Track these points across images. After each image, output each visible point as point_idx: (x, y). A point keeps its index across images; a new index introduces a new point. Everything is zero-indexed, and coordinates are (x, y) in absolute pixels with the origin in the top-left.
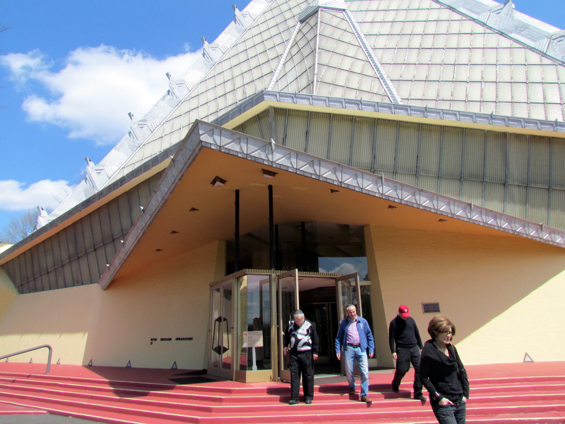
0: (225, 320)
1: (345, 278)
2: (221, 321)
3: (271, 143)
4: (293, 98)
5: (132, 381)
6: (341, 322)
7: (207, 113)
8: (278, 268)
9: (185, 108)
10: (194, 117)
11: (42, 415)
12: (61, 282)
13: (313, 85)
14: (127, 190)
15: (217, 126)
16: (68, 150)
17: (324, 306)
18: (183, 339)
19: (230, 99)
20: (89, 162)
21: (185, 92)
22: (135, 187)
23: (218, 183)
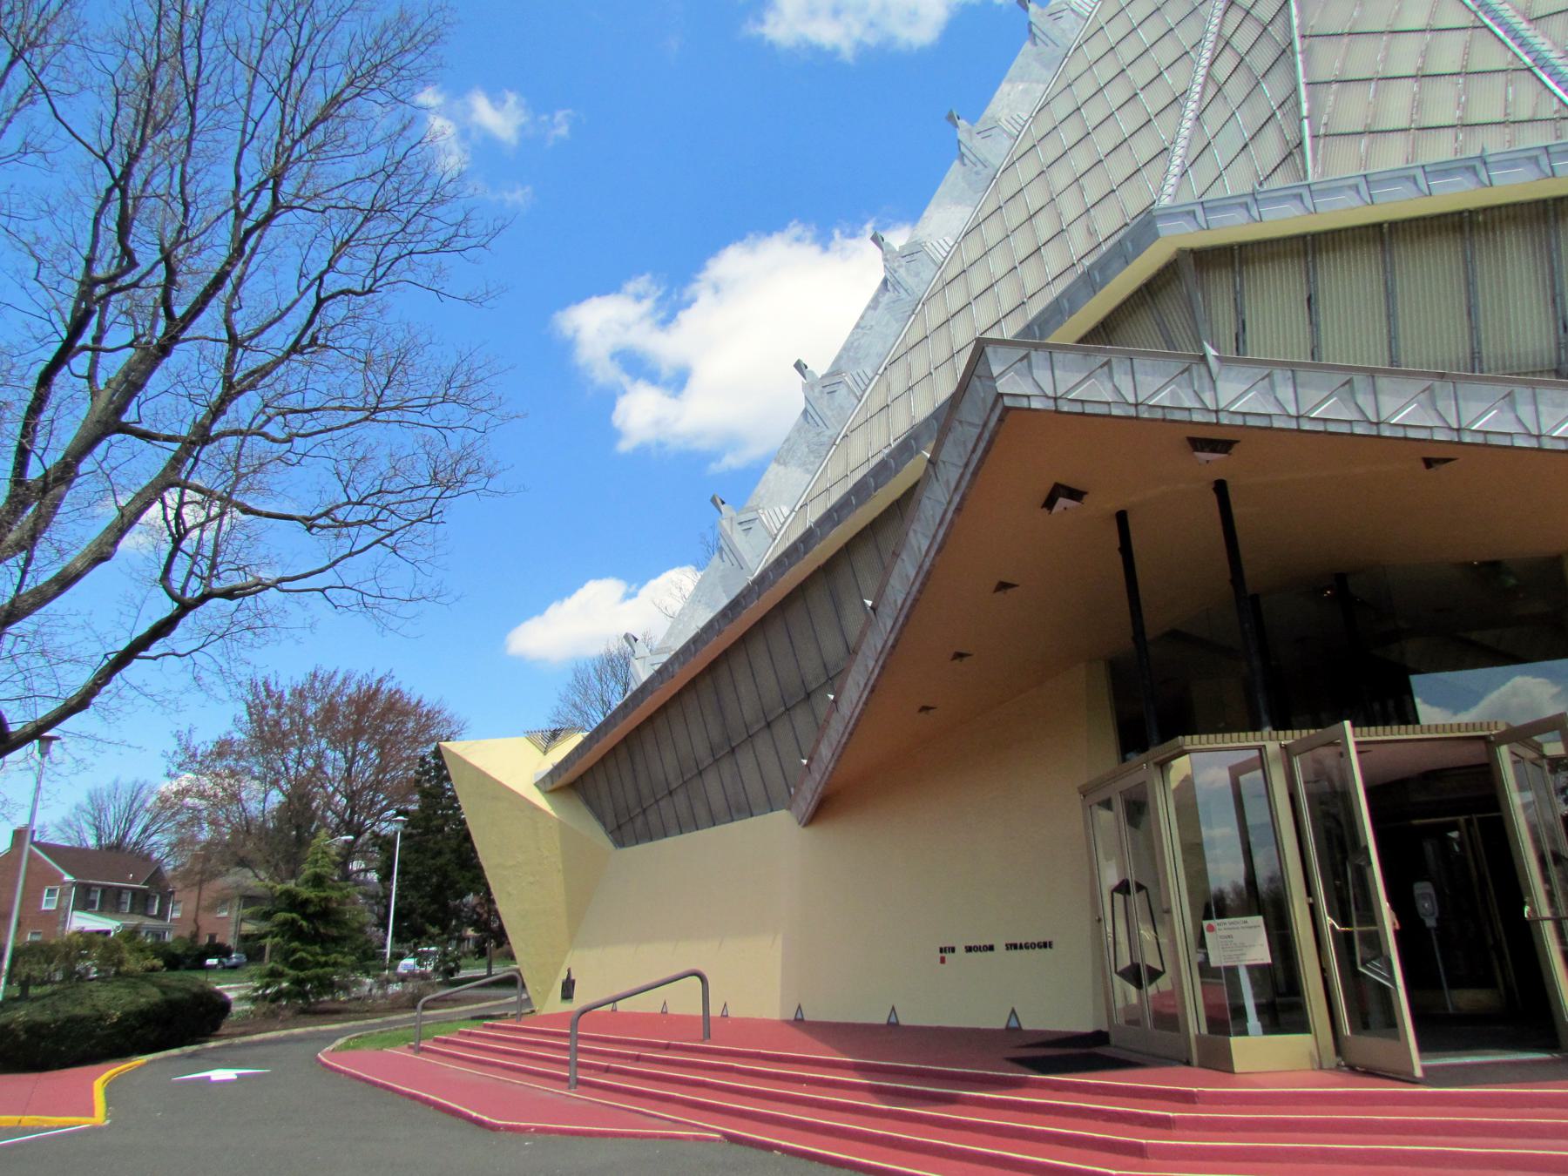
0: (1140, 887)
1: (1522, 735)
2: (1128, 892)
3: (1203, 358)
4: (1246, 206)
5: (915, 1063)
6: (1431, 922)
7: (999, 313)
8: (1282, 724)
9: (935, 315)
10: (963, 335)
11: (712, 1144)
12: (701, 812)
13: (1303, 154)
14: (822, 561)
15: (1034, 340)
16: (693, 489)
17: (1454, 826)
18: (1027, 946)
19: (1054, 260)
20: (723, 507)
21: (927, 273)
22: (840, 551)
23: (1062, 502)
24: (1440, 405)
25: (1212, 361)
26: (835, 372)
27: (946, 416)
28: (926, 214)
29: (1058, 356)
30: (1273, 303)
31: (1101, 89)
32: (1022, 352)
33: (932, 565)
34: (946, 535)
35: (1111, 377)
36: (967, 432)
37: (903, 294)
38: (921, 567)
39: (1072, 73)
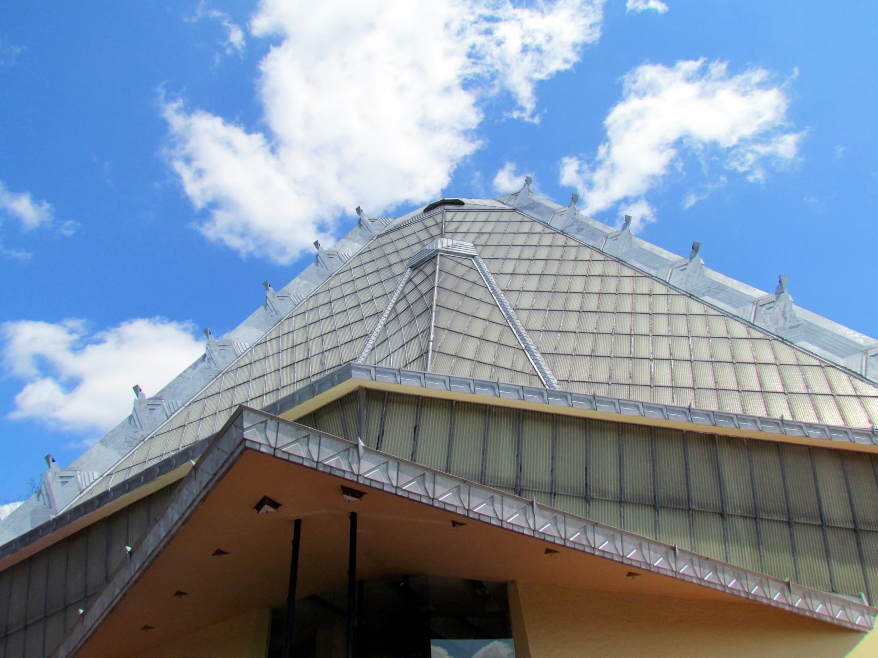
3: (357, 446)
7: (257, 394)
13: (427, 357)
15: (272, 413)
19: (300, 372)
20: (52, 464)
23: (267, 508)
24: (462, 496)
25: (361, 449)
26: (158, 398)
27: (217, 438)
28: (238, 327)
29: (282, 425)
30: (399, 426)
31: (343, 297)
32: (264, 419)
33: (177, 531)
34: (191, 514)
35: (308, 445)
36: (220, 455)
37: (213, 365)
38: (170, 531)
39: (332, 284)
